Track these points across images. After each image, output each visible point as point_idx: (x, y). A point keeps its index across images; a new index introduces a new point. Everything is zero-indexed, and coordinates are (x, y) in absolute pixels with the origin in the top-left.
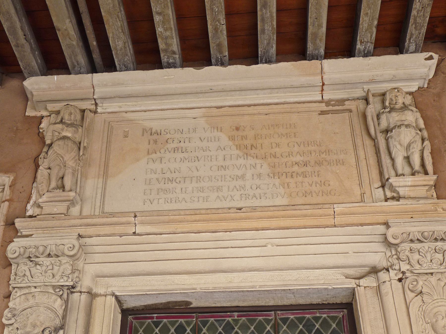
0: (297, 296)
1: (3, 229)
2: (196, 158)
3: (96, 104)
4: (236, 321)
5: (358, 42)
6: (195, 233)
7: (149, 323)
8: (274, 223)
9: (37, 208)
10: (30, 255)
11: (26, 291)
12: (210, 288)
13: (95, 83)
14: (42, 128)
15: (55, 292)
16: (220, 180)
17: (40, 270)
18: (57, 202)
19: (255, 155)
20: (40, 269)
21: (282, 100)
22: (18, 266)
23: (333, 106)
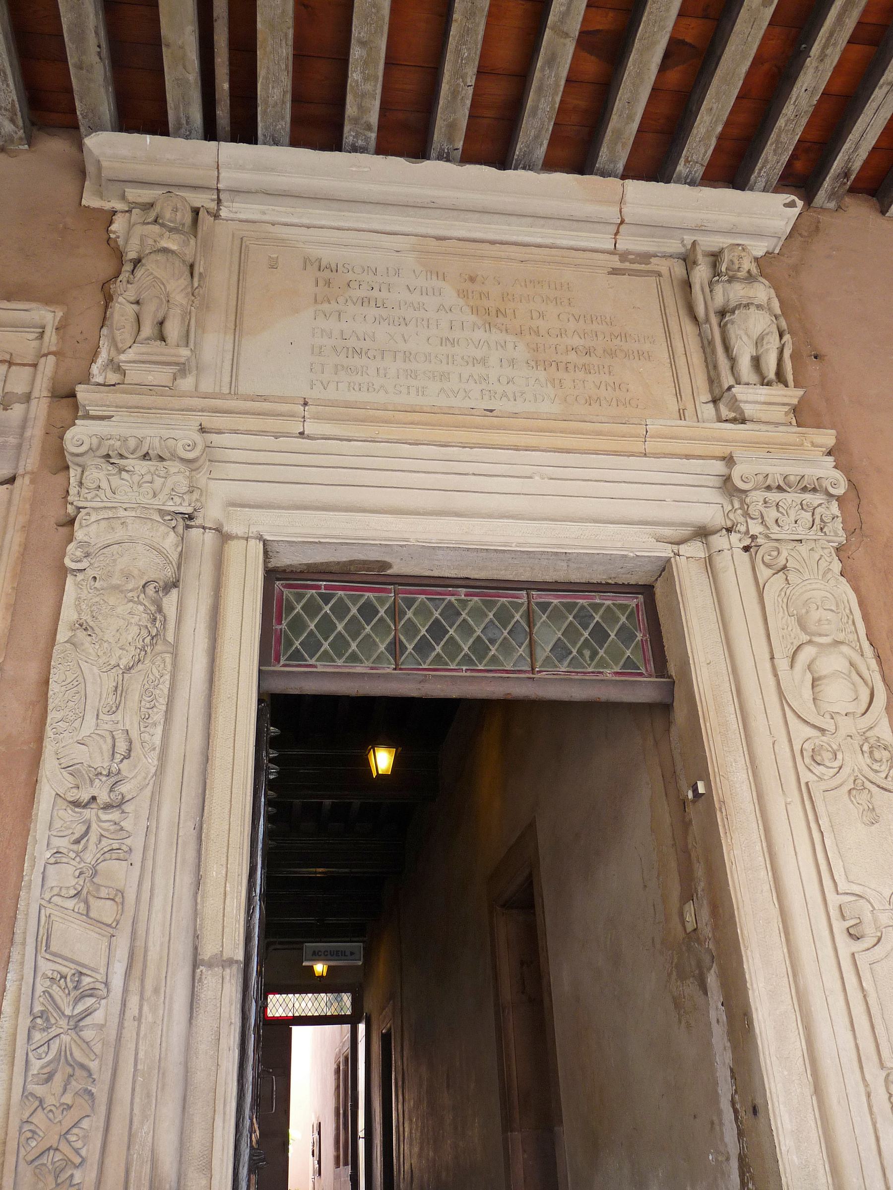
0: (572, 565)
1: (48, 404)
2: (402, 320)
3: (219, 201)
5: (682, 161)
6: (410, 444)
7: (312, 596)
8: (546, 440)
9: (111, 373)
10: (110, 453)
12: (434, 541)
14: (114, 232)
15: (164, 520)
16: (444, 361)
17: (128, 481)
19: (504, 326)
20: (129, 480)
21: (548, 241)
22: (83, 471)
23: (631, 263)
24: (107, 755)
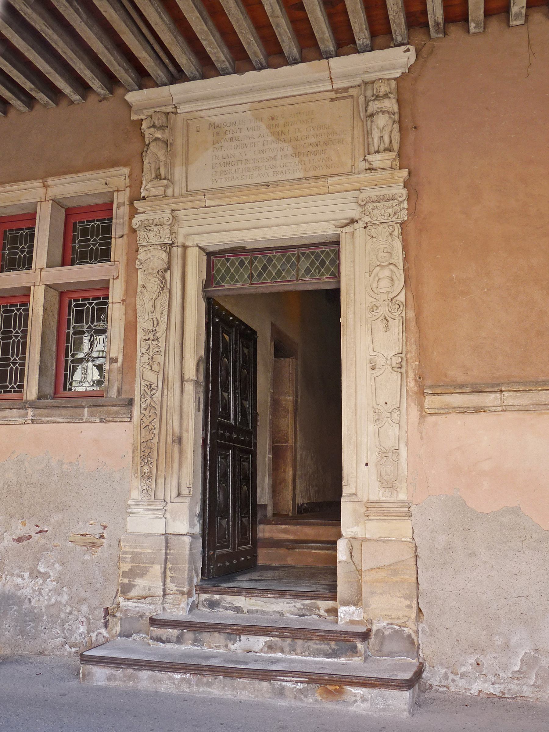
3: (176, 107)
4: (274, 256)
6: (242, 203)
8: (291, 193)
11: (146, 249)
13: (172, 93)
14: (143, 129)
18: (57, 333)
24: (152, 325)
